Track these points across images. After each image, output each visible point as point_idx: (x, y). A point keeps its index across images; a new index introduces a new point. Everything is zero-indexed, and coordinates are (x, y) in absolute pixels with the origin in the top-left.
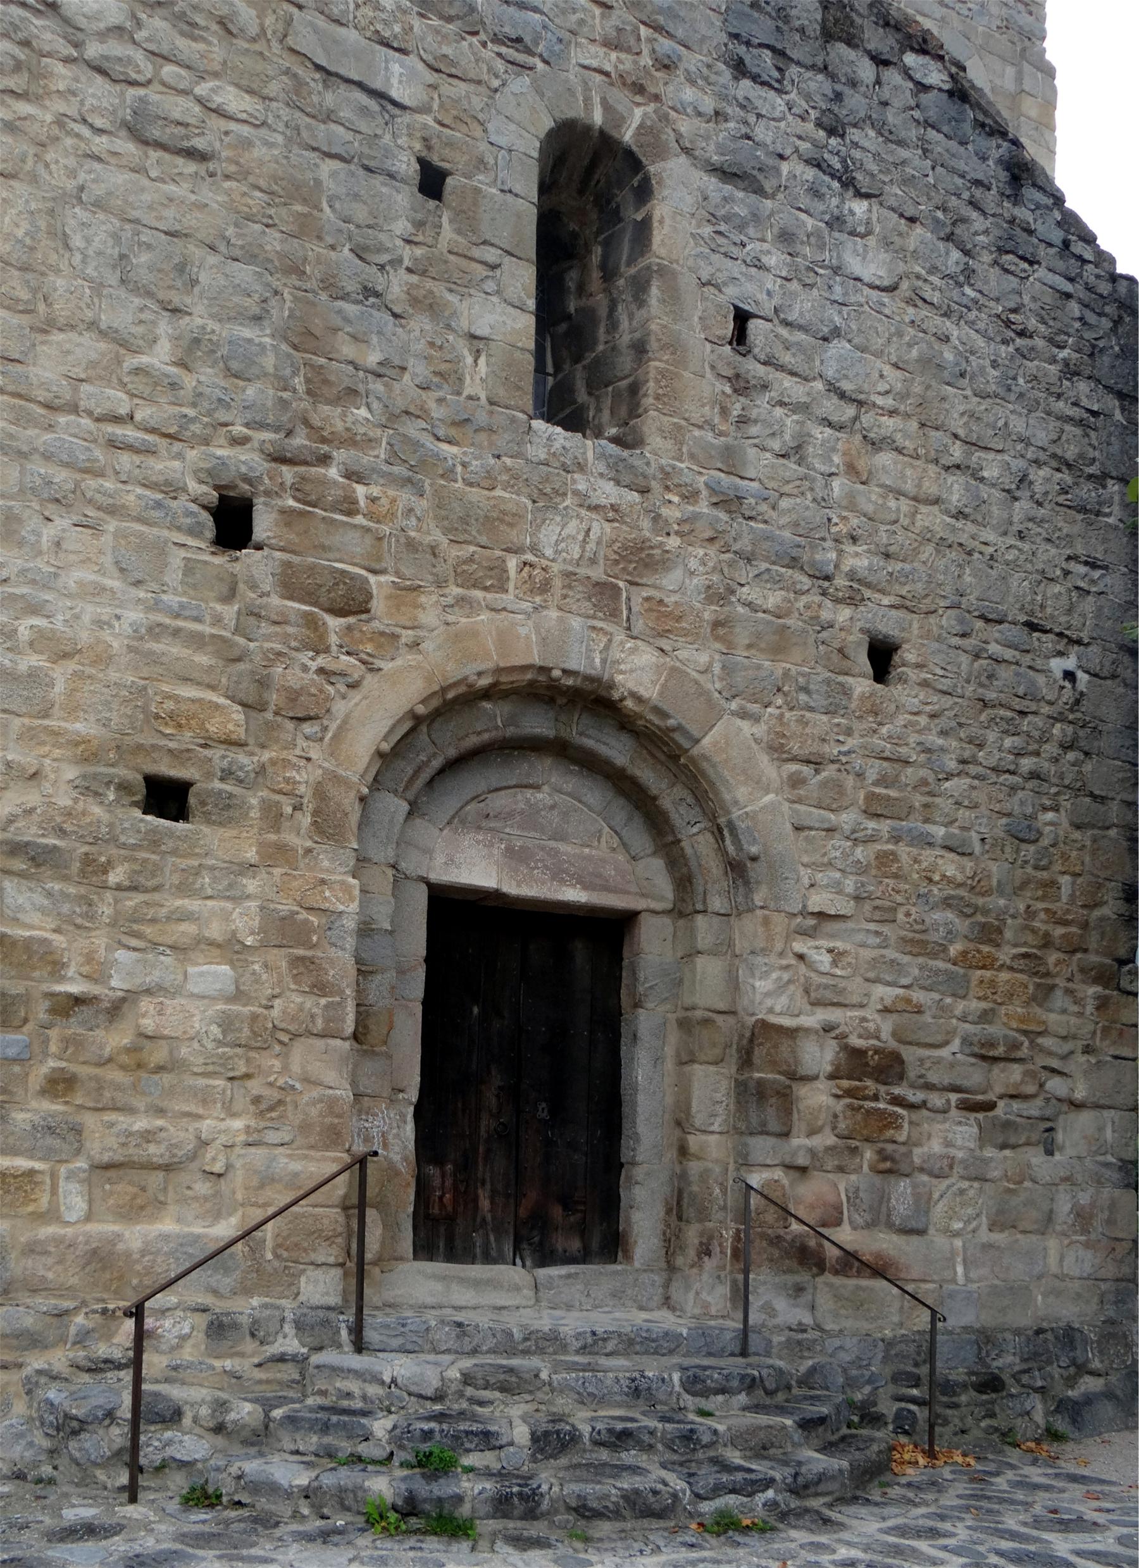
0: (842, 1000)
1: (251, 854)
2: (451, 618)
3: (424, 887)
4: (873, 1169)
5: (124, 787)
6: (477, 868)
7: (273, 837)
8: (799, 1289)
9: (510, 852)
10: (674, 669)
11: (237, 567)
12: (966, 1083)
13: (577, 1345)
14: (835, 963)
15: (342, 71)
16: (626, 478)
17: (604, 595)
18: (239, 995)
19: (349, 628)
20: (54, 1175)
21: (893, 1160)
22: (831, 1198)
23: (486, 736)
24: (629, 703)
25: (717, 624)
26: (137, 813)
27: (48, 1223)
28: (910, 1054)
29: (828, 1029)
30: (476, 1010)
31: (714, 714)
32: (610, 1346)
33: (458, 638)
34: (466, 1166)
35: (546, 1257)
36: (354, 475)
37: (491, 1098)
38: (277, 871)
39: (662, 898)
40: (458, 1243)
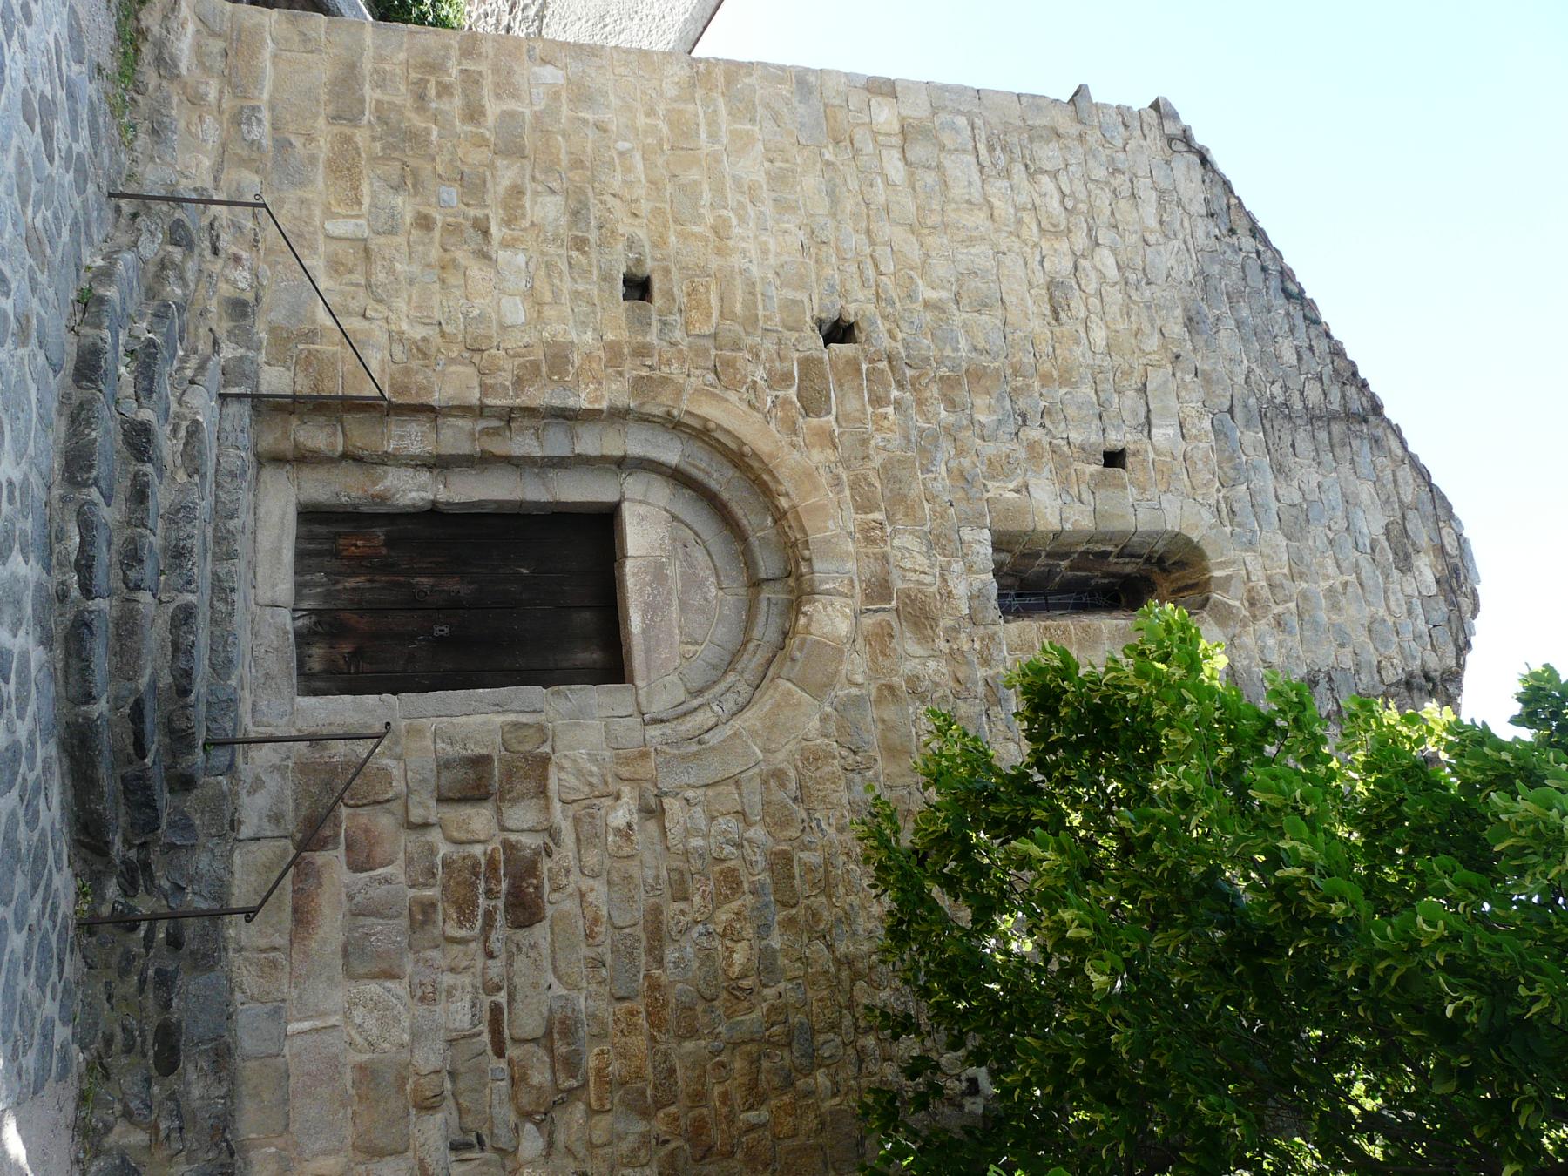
0: (584, 844)
1: (609, 336)
2: (821, 470)
3: (616, 499)
4: (414, 900)
5: (639, 262)
6: (642, 536)
7: (626, 351)
8: (276, 818)
9: (660, 567)
10: (841, 651)
11: (810, 333)
12: (517, 1006)
13: (222, 572)
14: (618, 831)
15: (1150, 400)
16: (975, 604)
17: (879, 590)
18: (504, 328)
19: (792, 402)
20: (357, 216)
21: (424, 923)
22: (379, 853)
23: (745, 522)
24: (802, 620)
25: (891, 687)
26: (624, 269)
27: (324, 213)
28: (540, 932)
29: (553, 833)
30: (525, 571)
31: (819, 690)
32: (219, 605)
33: (809, 475)
34: (386, 567)
35: (303, 639)
36: (898, 404)
37: (452, 585)
38: (602, 353)
39: (650, 703)
40: (313, 561)
